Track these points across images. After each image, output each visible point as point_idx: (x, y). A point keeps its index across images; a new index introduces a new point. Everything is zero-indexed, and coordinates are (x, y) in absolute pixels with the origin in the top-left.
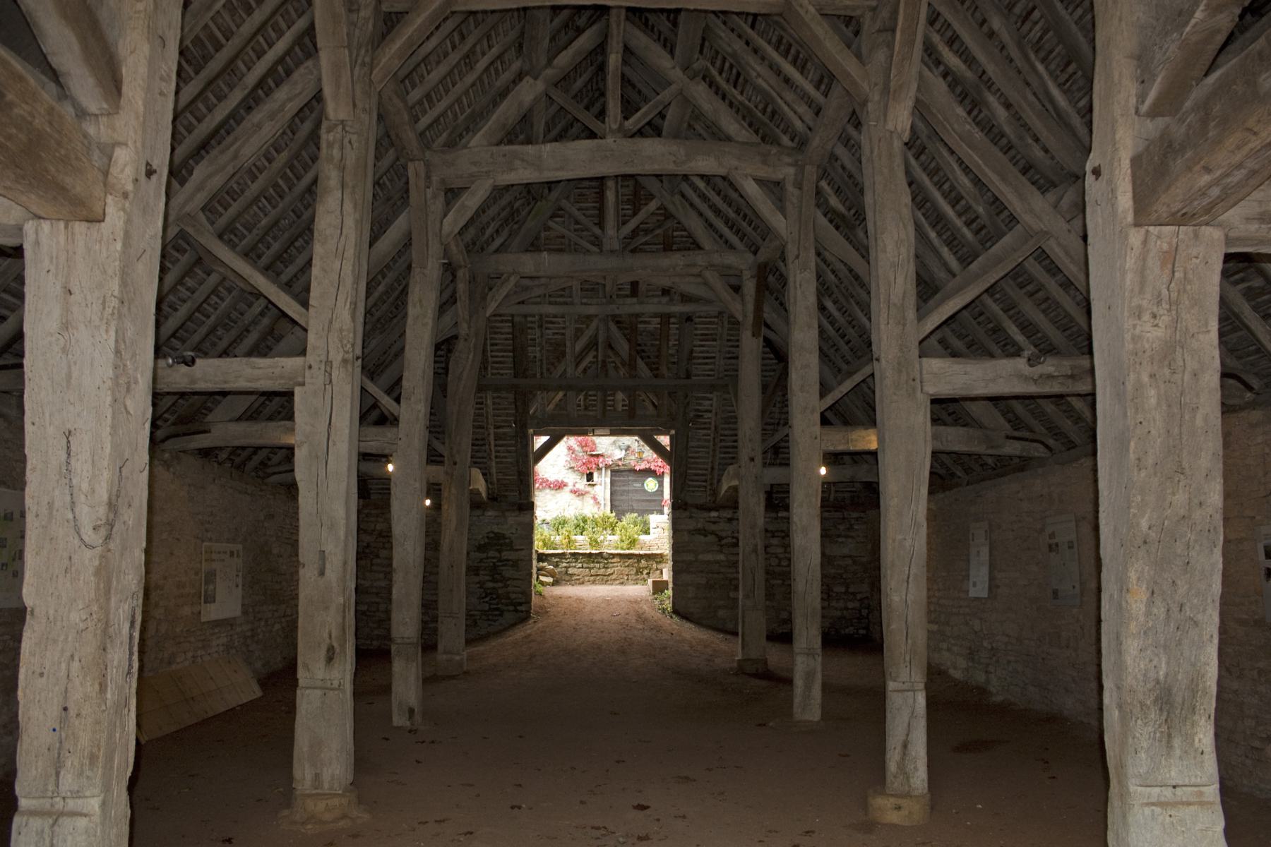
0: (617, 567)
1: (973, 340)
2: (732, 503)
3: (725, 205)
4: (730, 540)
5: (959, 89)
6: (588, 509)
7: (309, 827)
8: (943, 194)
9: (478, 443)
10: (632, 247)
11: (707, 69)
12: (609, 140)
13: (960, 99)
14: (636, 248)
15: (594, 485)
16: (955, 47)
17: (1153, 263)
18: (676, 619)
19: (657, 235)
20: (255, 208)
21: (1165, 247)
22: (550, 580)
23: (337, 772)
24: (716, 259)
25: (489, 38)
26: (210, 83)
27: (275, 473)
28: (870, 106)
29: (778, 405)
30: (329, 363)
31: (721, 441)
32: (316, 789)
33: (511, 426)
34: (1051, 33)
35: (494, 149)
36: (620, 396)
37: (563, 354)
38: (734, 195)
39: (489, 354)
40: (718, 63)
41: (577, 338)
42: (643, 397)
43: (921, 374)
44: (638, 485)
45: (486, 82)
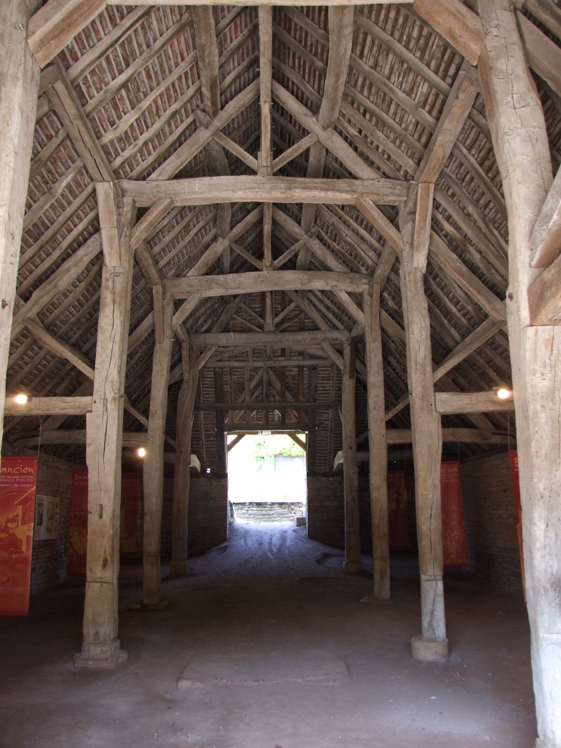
8: (449, 300)
12: (265, 272)
17: (541, 346)
20: (67, 312)
21: (547, 337)
23: (108, 631)
26: (41, 247)
30: (105, 400)
33: (214, 430)
34: (500, 215)
35: (201, 277)
36: (277, 412)
39: (201, 389)
40: (325, 229)
41: (251, 380)
45: (196, 241)
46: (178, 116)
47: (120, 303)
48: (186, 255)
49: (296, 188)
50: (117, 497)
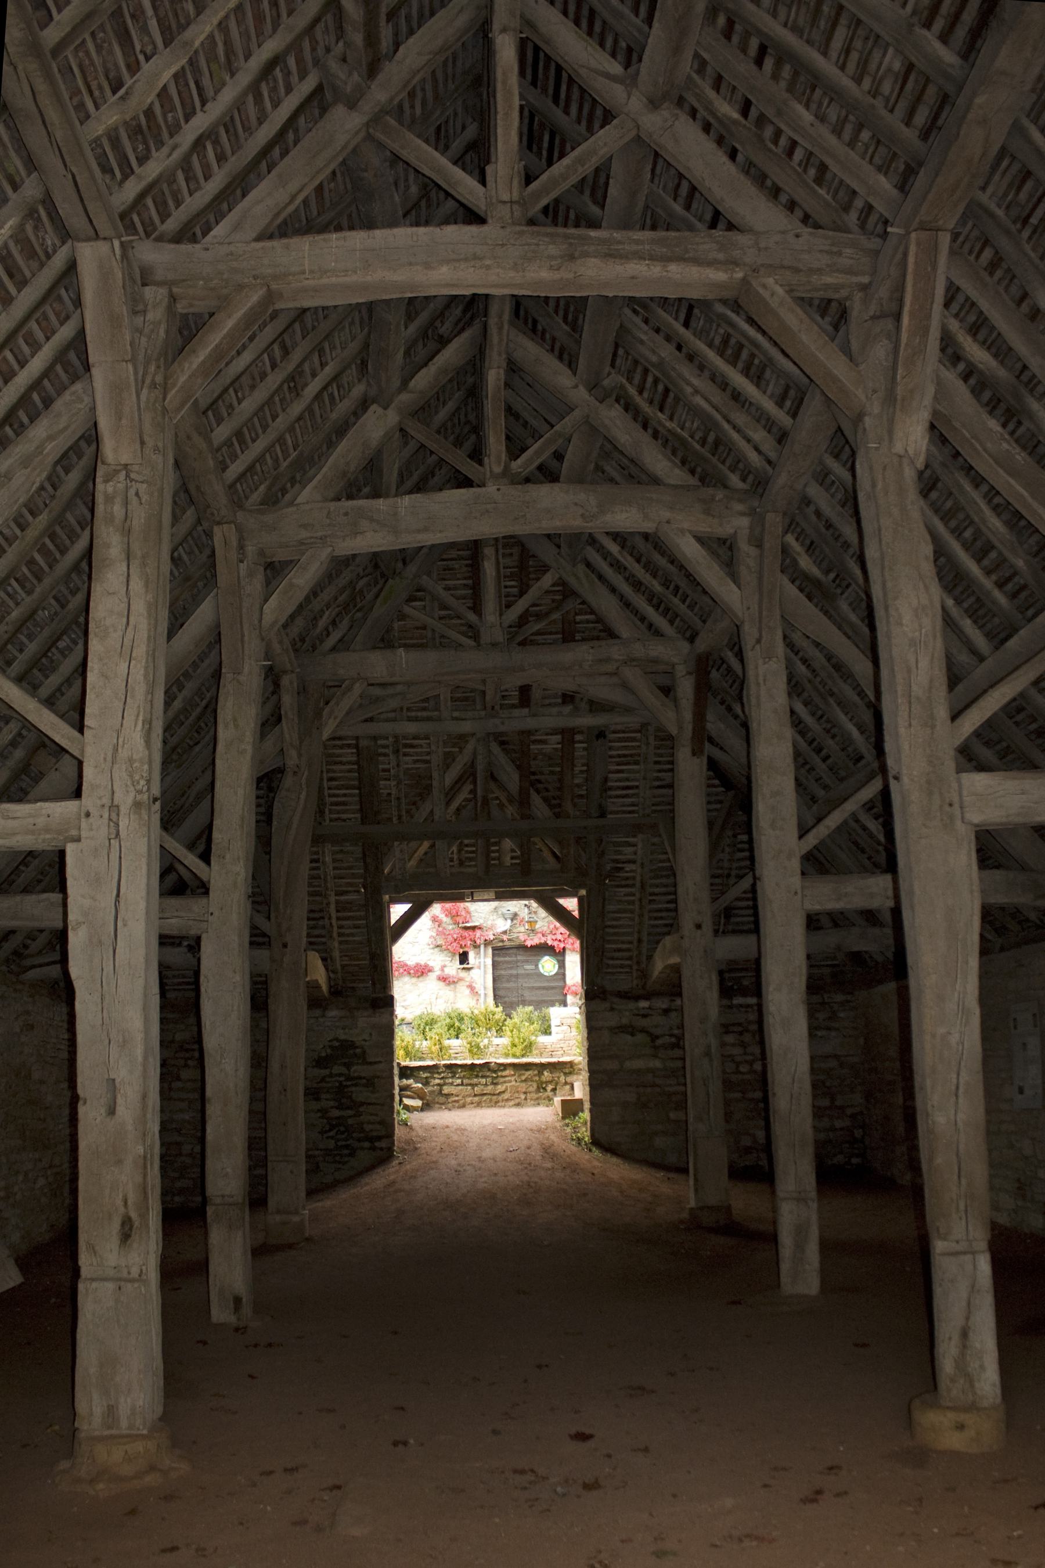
0: (510, 1082)
1: (1008, 747)
2: (672, 986)
3: (648, 576)
4: (667, 1040)
5: (987, 395)
6: (464, 1002)
7: (101, 1486)
9: (316, 916)
10: (520, 638)
11: (622, 387)
12: (491, 489)
13: (989, 409)
14: (526, 639)
15: (469, 969)
16: (982, 334)
18: (596, 1152)
19: (554, 621)
22: (418, 1103)
24: (638, 650)
25: (321, 353)
27: (34, 967)
28: (868, 421)
29: (727, 849)
30: (114, 808)
31: (650, 901)
32: (109, 1428)
33: (358, 892)
35: (333, 505)
36: (508, 844)
37: (429, 788)
38: (662, 562)
39: (326, 792)
40: (637, 378)
42: (540, 845)
43: (960, 795)
44: (529, 967)
46: (278, 72)
47: (144, 557)
48: (291, 450)
49: (586, 255)
50: (151, 1060)
